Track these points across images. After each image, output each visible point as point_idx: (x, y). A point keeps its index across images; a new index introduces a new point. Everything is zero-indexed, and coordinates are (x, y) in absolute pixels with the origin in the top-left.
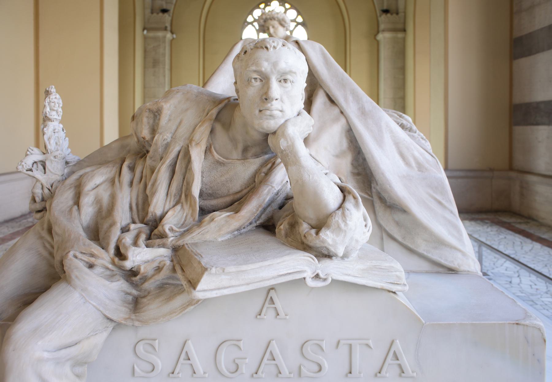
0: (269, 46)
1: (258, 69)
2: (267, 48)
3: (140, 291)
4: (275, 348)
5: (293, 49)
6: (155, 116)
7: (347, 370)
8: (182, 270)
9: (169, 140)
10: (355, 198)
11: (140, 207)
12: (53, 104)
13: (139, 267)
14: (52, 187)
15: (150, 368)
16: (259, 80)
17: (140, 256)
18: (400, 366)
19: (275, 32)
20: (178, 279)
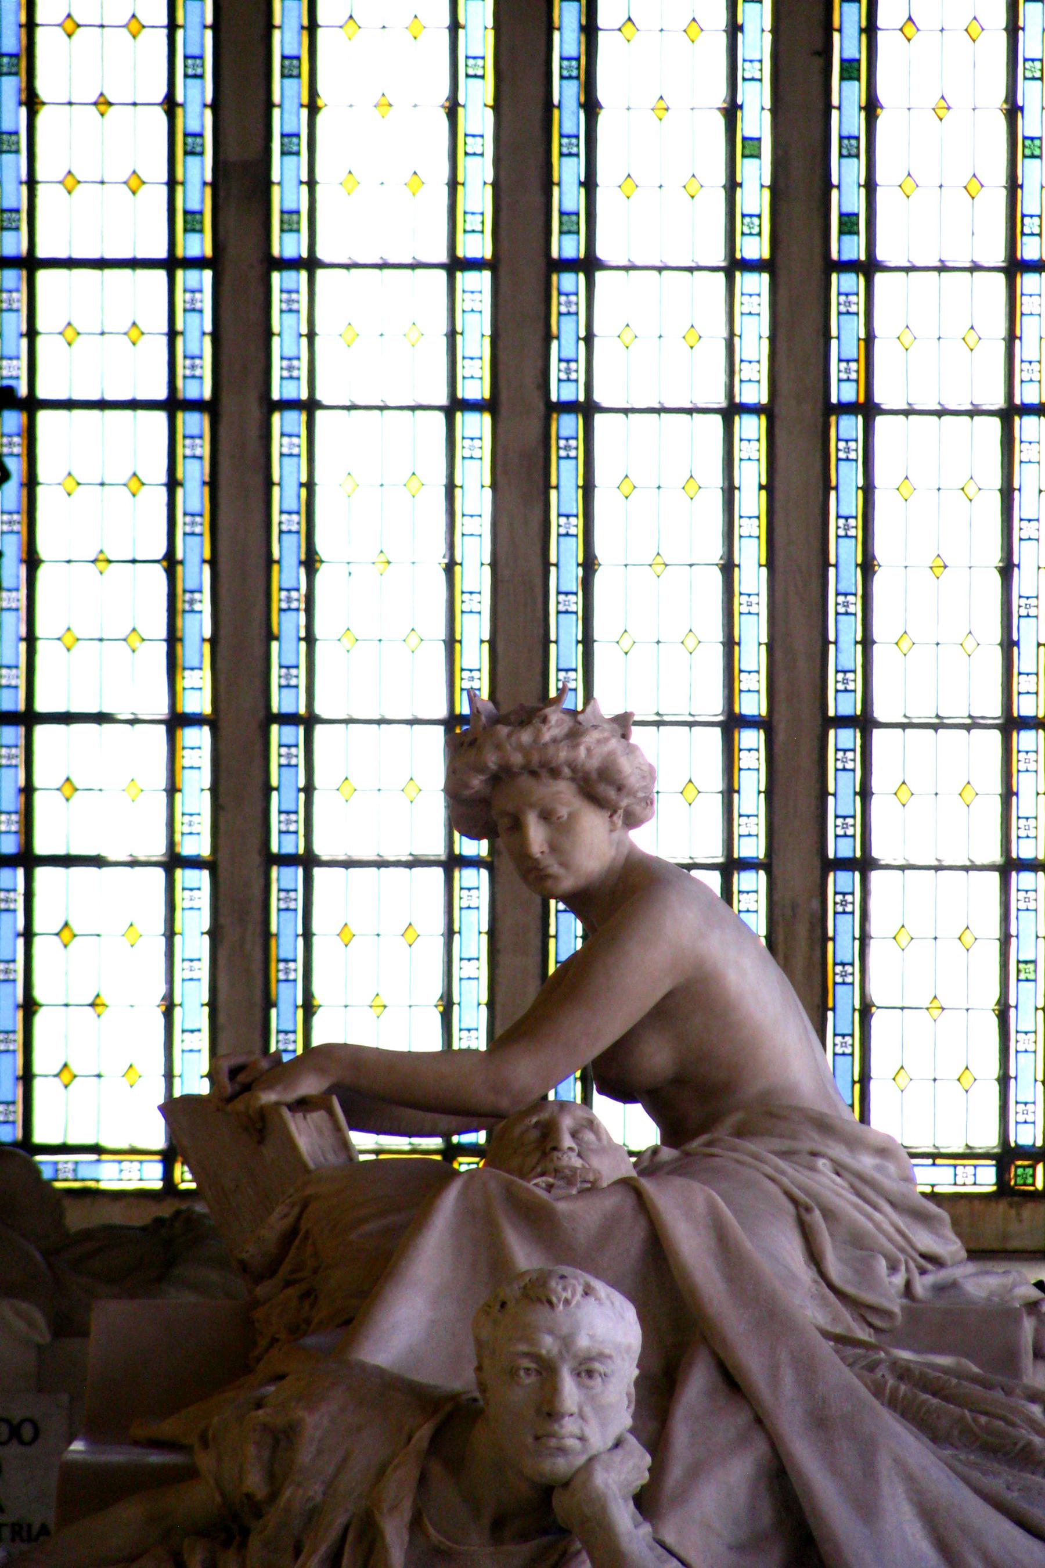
0: (554, 1300)
1: (532, 1350)
2: (550, 1303)
5: (608, 1297)
6: (277, 1442)
9: (318, 1499)
16: (534, 1373)
19: (554, 848)
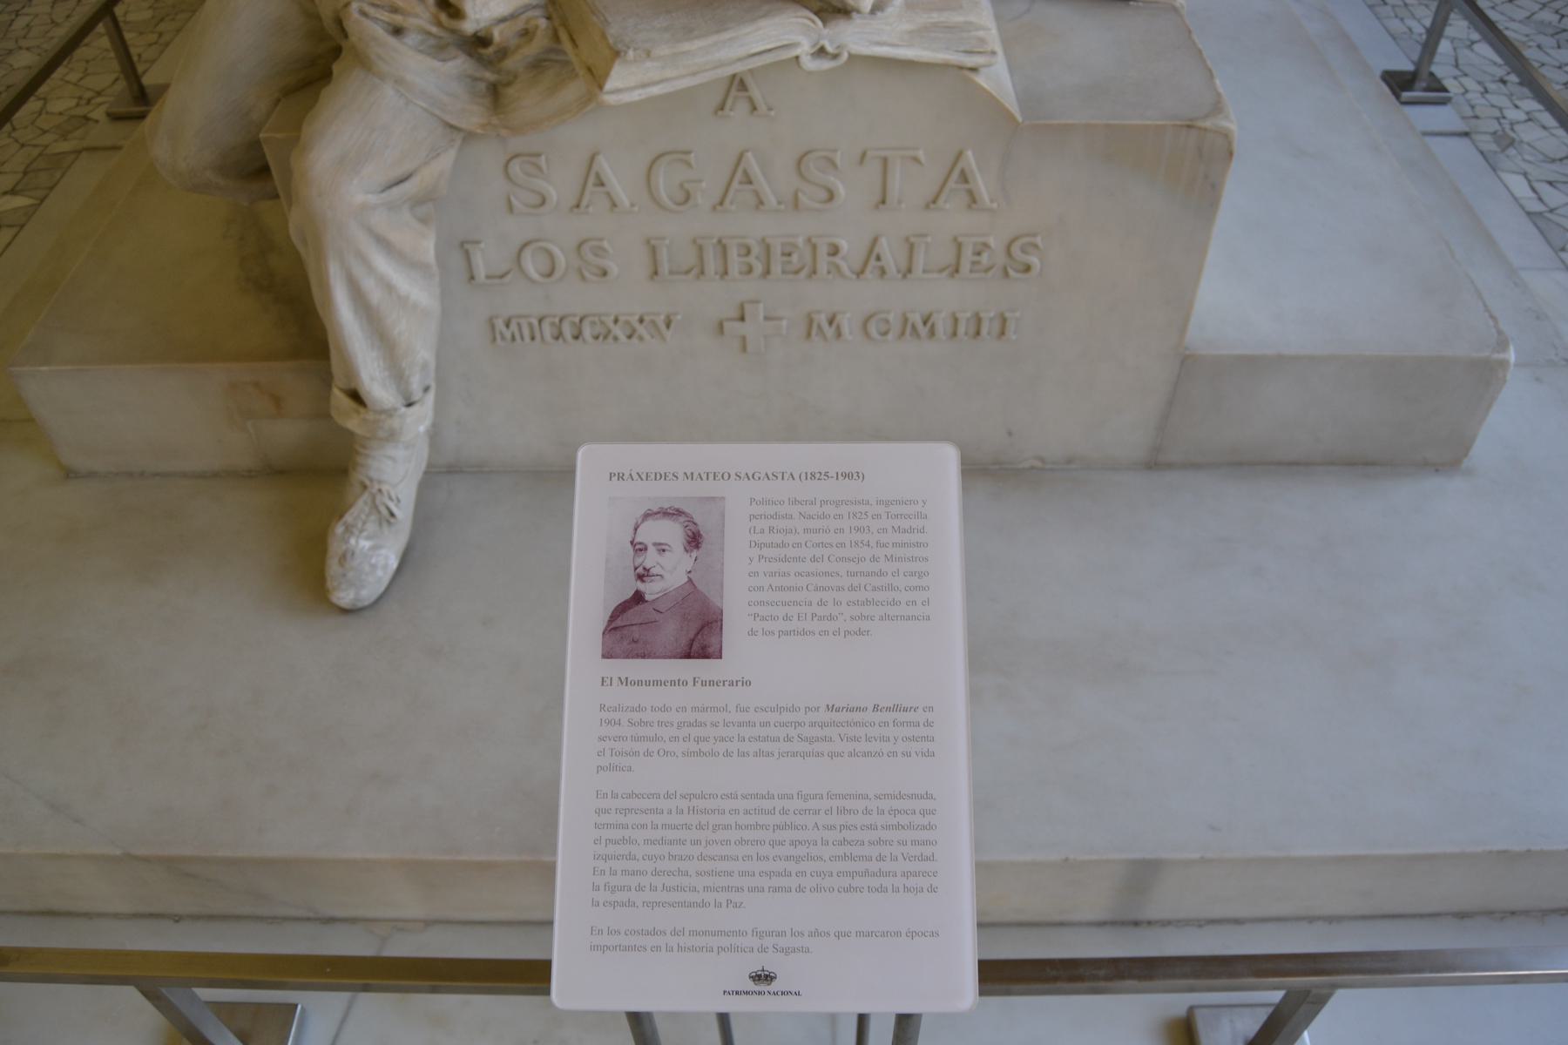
3: (499, 72)
4: (751, 160)
8: (573, 40)
13: (488, 29)
15: (538, 200)
18: (970, 193)
20: (565, 53)
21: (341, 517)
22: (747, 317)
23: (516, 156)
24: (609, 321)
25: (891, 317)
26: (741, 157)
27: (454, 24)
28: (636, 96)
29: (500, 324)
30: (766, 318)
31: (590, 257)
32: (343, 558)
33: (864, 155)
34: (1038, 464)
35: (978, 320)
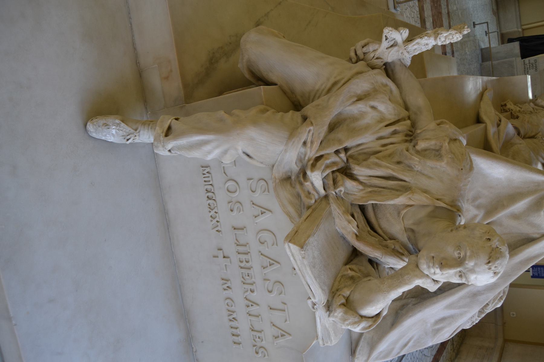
0: (490, 264)
1: (467, 257)
2: (489, 262)
4: (276, 266)
6: (437, 151)
7: (272, 307)
10: (370, 326)
11: (361, 151)
12: (451, 37)
14: (377, 58)
15: (254, 190)
17: (316, 178)
18: (278, 337)
21: (123, 121)
22: (225, 259)
23: (267, 183)
24: (215, 210)
25: (233, 307)
26: (279, 263)
27: (309, 166)
28: (289, 253)
29: (208, 170)
30: (226, 265)
31: (236, 207)
32: (106, 125)
33: (285, 304)
34: (194, 350)
35: (238, 336)
